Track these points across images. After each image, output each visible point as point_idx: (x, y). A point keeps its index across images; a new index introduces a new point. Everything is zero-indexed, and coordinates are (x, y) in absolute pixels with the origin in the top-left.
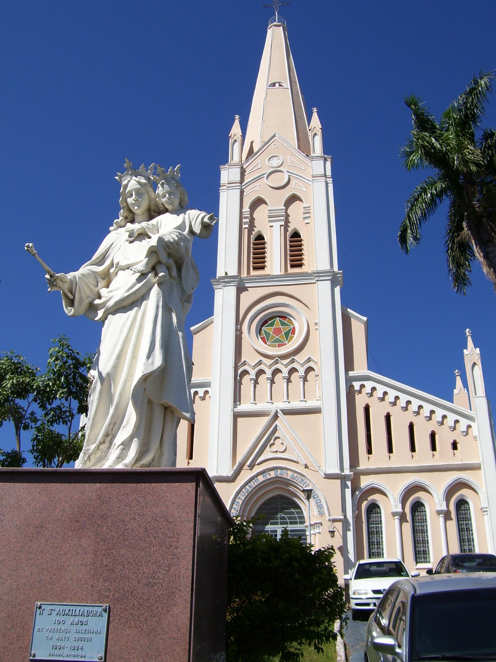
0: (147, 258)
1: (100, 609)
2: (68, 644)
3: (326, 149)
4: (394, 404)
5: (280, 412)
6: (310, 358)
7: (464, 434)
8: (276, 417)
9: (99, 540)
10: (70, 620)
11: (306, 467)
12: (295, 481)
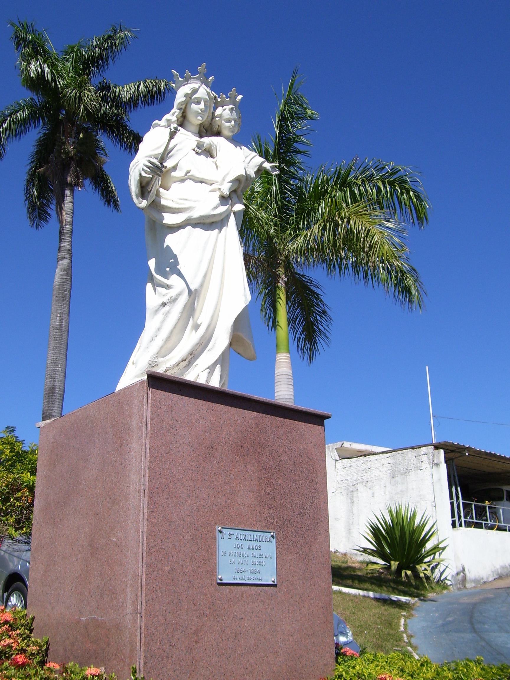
0: (231, 184)
1: (269, 535)
2: (248, 568)
9: (261, 468)
10: (247, 544)
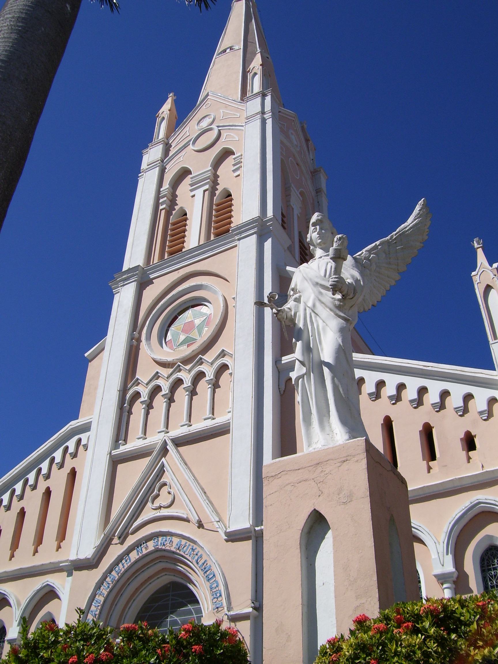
3: (266, 83)
4: (397, 398)
5: (169, 442)
6: (223, 351)
7: (485, 416)
8: (164, 451)
11: (200, 525)
12: (182, 553)
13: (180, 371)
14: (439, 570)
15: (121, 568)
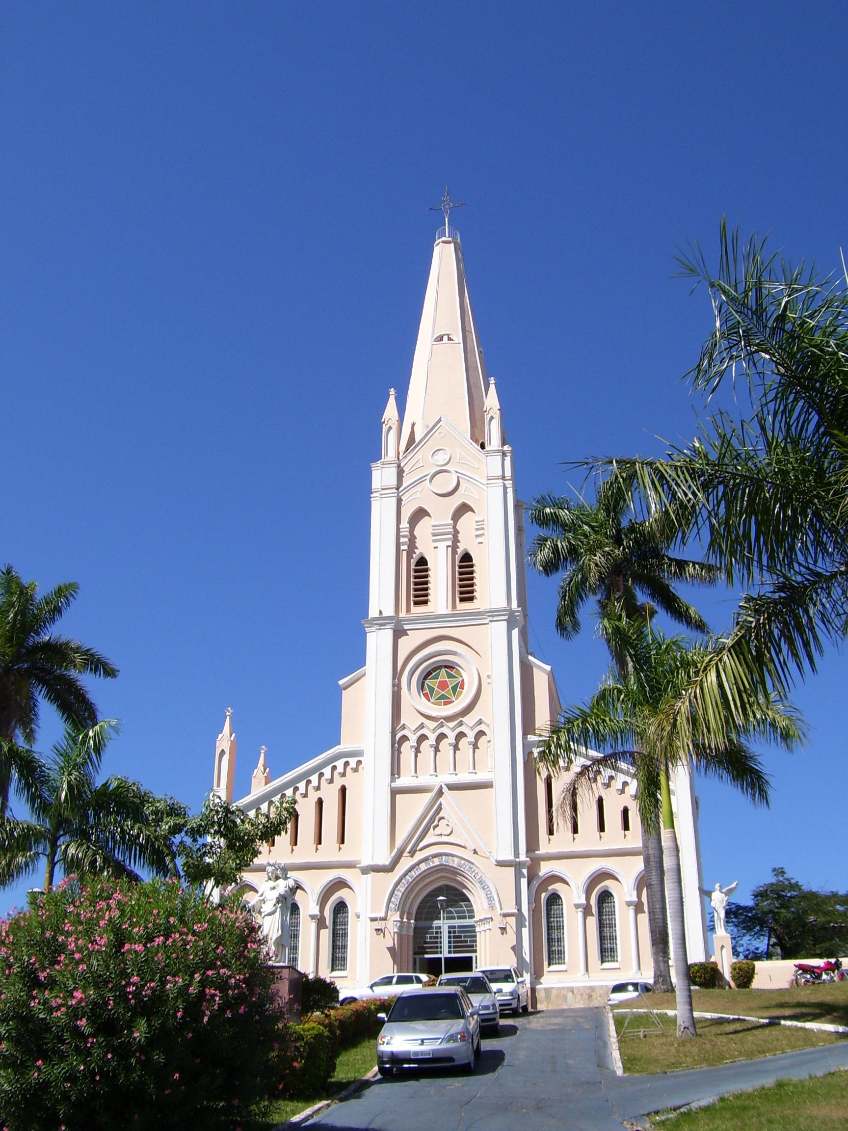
8: (440, 793)
13: (442, 726)
14: (629, 899)
15: (414, 874)
